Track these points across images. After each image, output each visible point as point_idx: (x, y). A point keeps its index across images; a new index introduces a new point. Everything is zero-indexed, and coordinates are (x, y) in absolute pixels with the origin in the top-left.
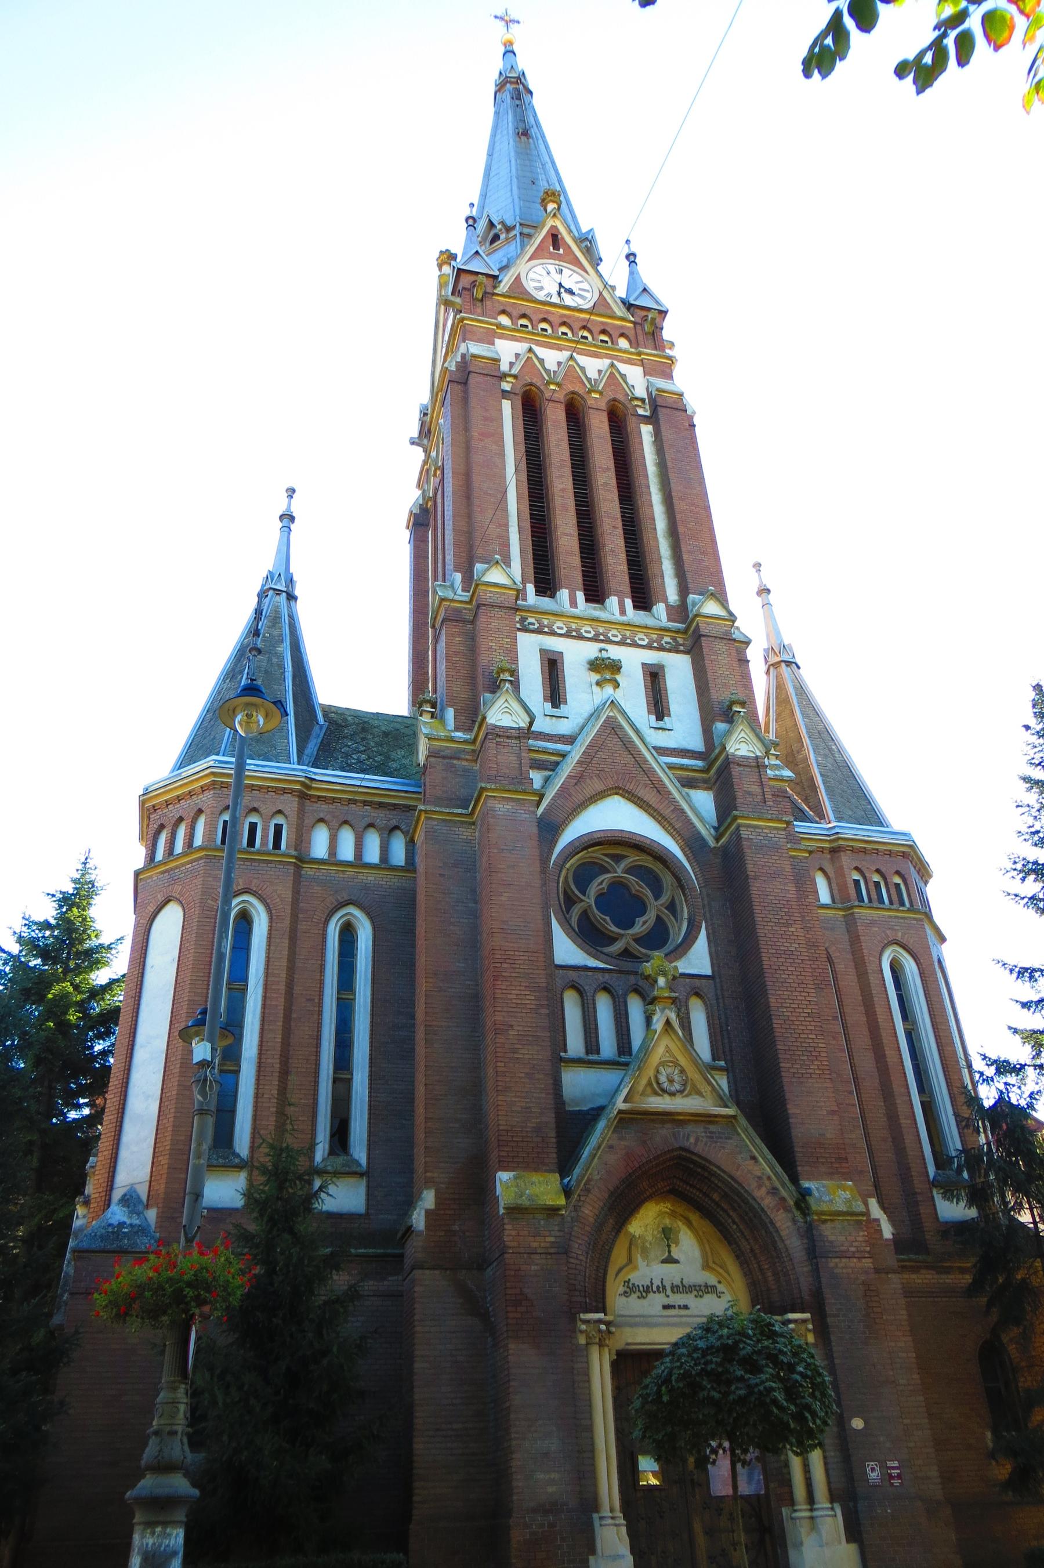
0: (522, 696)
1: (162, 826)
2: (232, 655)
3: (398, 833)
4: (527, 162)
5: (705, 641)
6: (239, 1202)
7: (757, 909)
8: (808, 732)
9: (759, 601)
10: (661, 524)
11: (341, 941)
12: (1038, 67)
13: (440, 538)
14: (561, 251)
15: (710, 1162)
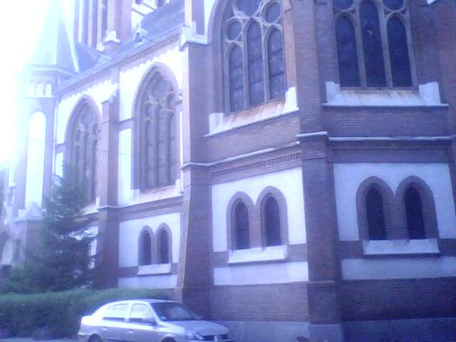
2: (213, 8)
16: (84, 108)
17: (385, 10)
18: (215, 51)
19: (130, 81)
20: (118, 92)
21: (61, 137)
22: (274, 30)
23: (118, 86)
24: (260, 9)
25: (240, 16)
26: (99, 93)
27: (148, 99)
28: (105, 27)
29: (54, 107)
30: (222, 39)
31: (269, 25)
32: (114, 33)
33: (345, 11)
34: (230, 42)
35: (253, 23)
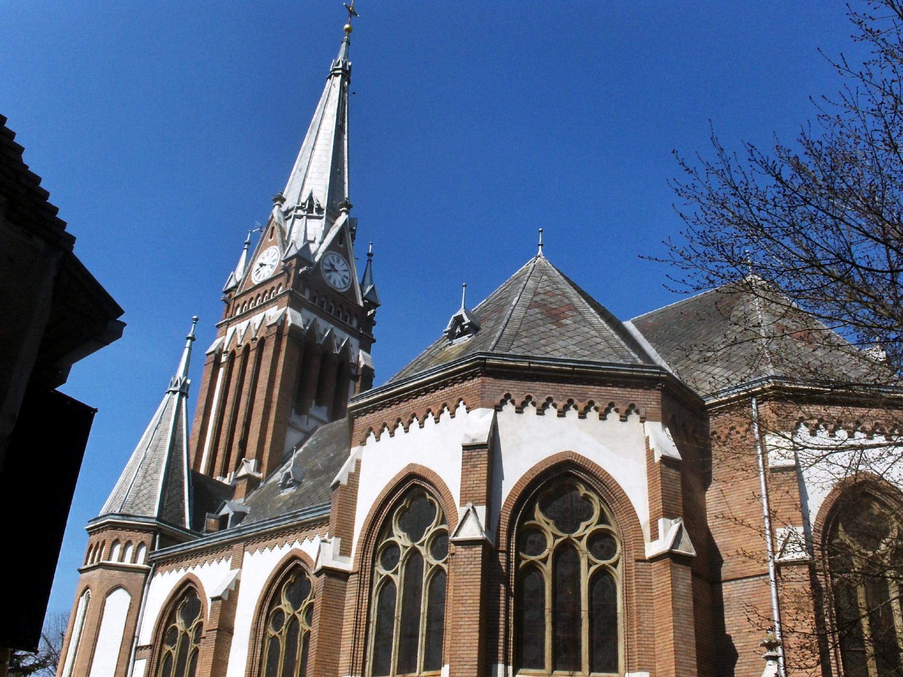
0: (109, 600)
1: (238, 306)
2: (369, 515)
3: (120, 592)
4: (579, 318)
5: (353, 574)
6: (339, 539)
7: (476, 643)
8: (643, 332)
9: (367, 258)
10: (184, 432)
11: (266, 430)
12: (457, 356)
13: (221, 452)
14: (342, 246)
15: (149, 584)
16: (187, 593)
17: (589, 559)
18: (361, 584)
19: (260, 566)
20: (237, 582)
21: (146, 637)
22: (438, 570)
23: (239, 574)
24: (426, 537)
25: (400, 538)
26: (212, 576)
27: (280, 603)
28: (242, 453)
29: (146, 583)
30: (373, 566)
31: (435, 562)
32: (253, 462)
33: (533, 558)
34: (385, 573)
35: (414, 552)
